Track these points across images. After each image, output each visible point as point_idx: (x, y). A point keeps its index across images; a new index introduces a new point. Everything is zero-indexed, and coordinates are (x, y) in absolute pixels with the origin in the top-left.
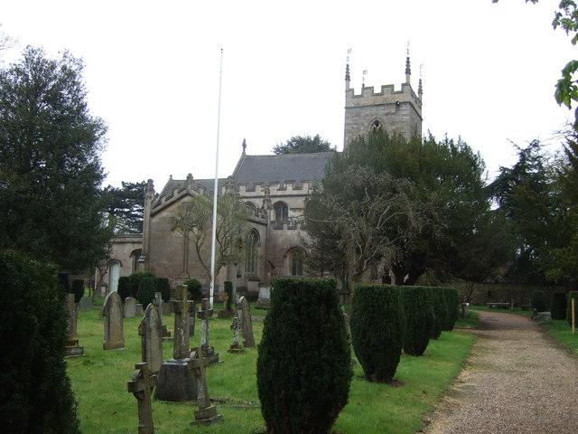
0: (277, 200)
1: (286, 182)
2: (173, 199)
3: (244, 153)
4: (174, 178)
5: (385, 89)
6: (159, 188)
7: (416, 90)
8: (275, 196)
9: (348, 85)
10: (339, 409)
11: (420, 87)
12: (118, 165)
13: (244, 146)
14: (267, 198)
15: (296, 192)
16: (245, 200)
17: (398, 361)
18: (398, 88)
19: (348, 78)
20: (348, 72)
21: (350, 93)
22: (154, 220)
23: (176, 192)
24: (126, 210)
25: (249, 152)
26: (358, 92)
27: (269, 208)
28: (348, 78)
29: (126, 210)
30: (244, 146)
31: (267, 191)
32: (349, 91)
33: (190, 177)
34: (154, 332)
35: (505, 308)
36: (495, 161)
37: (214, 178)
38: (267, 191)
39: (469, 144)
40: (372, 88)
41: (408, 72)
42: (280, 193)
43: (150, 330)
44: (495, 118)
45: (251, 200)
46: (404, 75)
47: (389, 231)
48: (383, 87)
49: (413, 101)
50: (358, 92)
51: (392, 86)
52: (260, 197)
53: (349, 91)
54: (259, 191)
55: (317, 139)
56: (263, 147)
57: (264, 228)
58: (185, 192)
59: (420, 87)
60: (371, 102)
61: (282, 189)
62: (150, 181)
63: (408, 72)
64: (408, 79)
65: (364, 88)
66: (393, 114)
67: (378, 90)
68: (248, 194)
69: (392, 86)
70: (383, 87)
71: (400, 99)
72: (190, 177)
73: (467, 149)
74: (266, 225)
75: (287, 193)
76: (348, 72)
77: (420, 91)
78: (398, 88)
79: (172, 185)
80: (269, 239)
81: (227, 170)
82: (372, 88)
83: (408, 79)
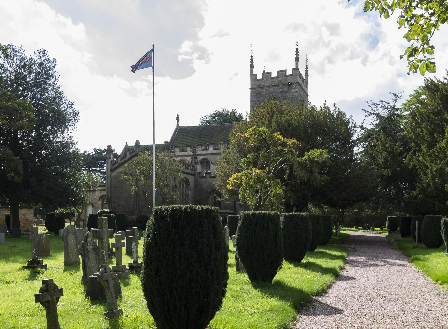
0: (203, 157)
1: (209, 145)
2: (126, 159)
3: (178, 124)
4: (129, 145)
5: (280, 73)
6: (119, 151)
7: (303, 73)
8: (201, 155)
9: (252, 71)
10: (211, 319)
11: (307, 71)
12: (84, 137)
13: (178, 119)
14: (194, 156)
15: (216, 151)
16: (179, 159)
17: (155, 320)
18: (289, 72)
19: (252, 66)
20: (252, 62)
21: (254, 77)
22: (114, 174)
23: (128, 153)
24: (99, 169)
25: (181, 124)
26: (260, 77)
27: (196, 163)
28: (252, 66)
29: (99, 169)
30: (178, 119)
31: (194, 152)
32: (253, 76)
33: (137, 142)
34: (92, 252)
35: (369, 228)
36: (362, 121)
37: (151, 143)
38: (194, 152)
39: (342, 110)
40: (270, 73)
41: (297, 59)
42: (204, 152)
43: (89, 251)
44: (363, 79)
45: (185, 158)
46: (294, 63)
47: (32, 60)
48: (278, 72)
49: (300, 81)
50: (260, 77)
51: (285, 71)
52: (190, 155)
53: (253, 76)
54: (189, 152)
55: (233, 112)
56: (192, 120)
57: (193, 177)
58: (134, 154)
59: (307, 71)
60: (269, 84)
61: (206, 149)
62: (109, 147)
63: (297, 59)
64: (297, 65)
65: (264, 74)
66: (286, 92)
67: (274, 75)
68: (181, 154)
69: (285, 71)
70: (278, 72)
71: (290, 80)
72: (137, 142)
73: (340, 114)
74: (194, 175)
75: (209, 152)
76: (252, 62)
77: (307, 74)
78: (289, 72)
79: (127, 149)
80: (197, 185)
81: (165, 135)
82: (270, 73)
83: (297, 65)
